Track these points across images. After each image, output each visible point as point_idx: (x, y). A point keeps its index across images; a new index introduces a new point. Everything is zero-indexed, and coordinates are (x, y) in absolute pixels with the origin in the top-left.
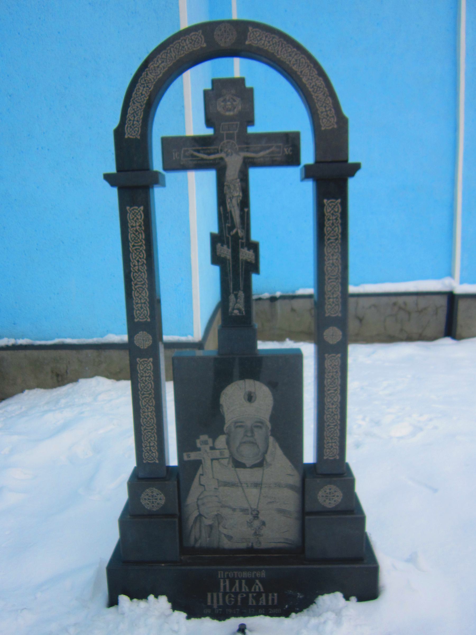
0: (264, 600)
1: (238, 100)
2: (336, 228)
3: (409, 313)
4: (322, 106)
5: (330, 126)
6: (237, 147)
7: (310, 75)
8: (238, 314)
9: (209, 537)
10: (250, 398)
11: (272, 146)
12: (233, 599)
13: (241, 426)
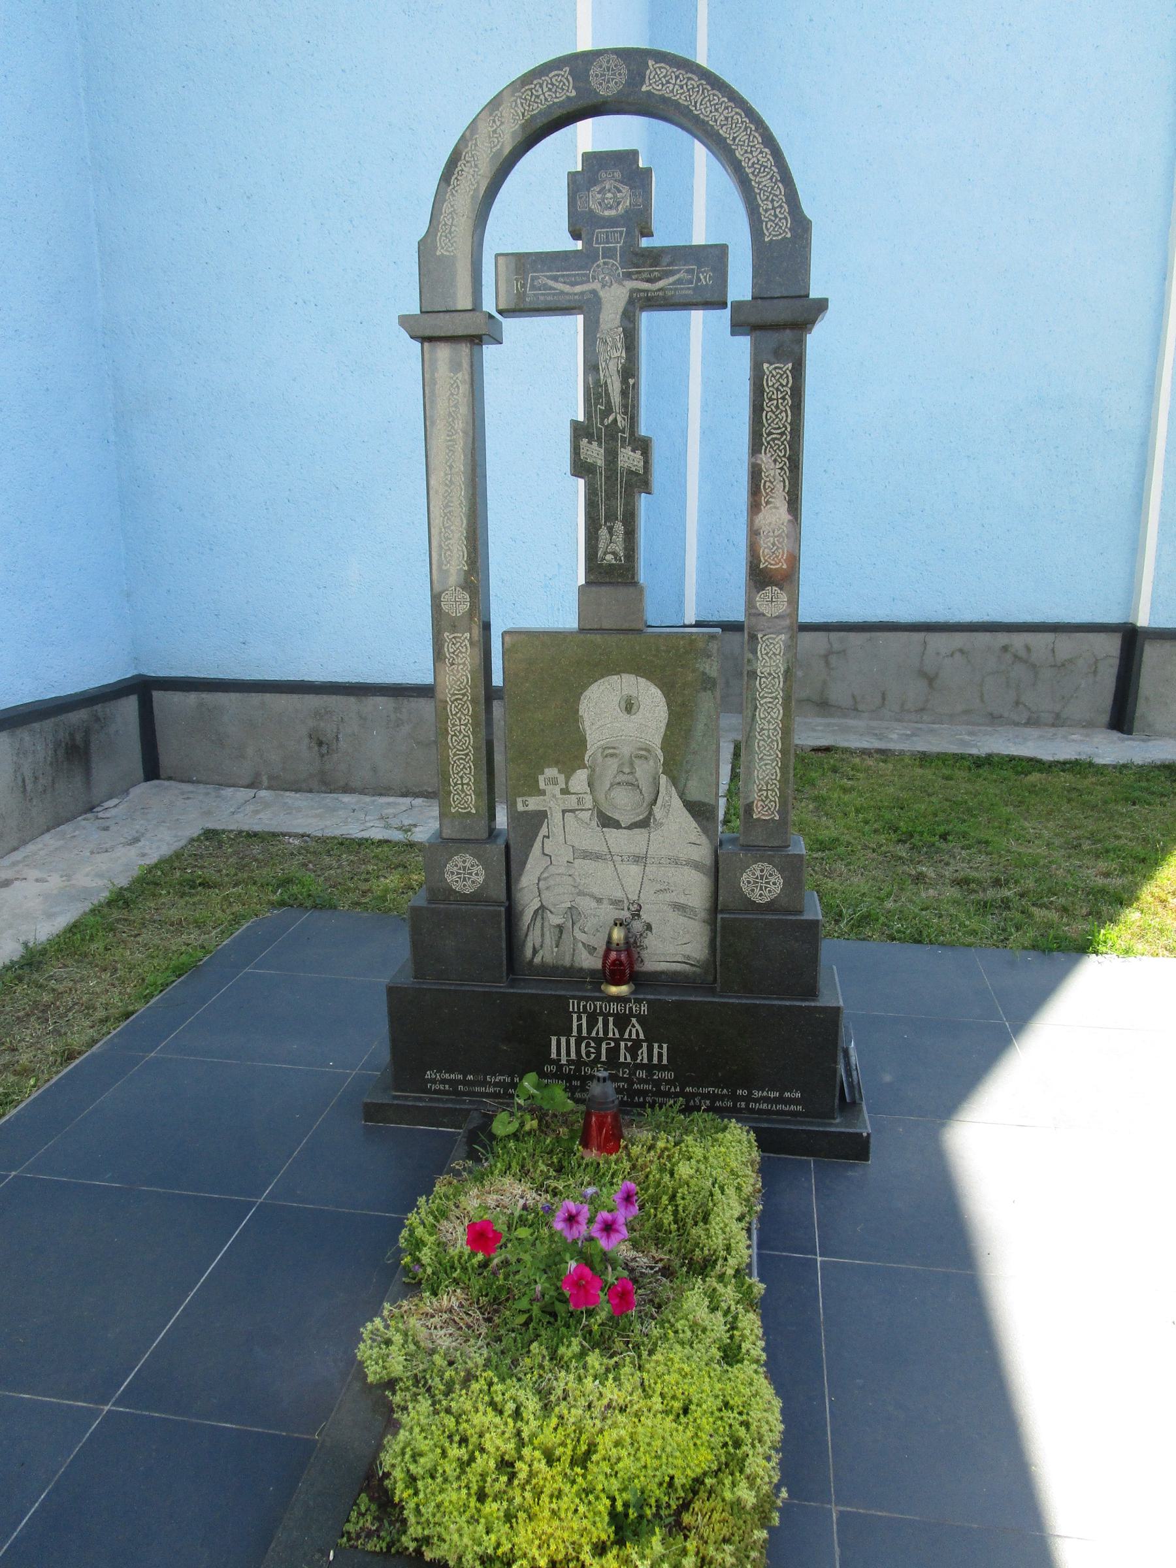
0: (645, 1055)
1: (625, 189)
2: (784, 414)
3: (1034, 668)
4: (767, 199)
5: (781, 234)
6: (620, 271)
7: (748, 145)
8: (614, 562)
9: (557, 947)
10: (629, 706)
11: (679, 271)
12: (593, 1050)
13: (612, 755)
